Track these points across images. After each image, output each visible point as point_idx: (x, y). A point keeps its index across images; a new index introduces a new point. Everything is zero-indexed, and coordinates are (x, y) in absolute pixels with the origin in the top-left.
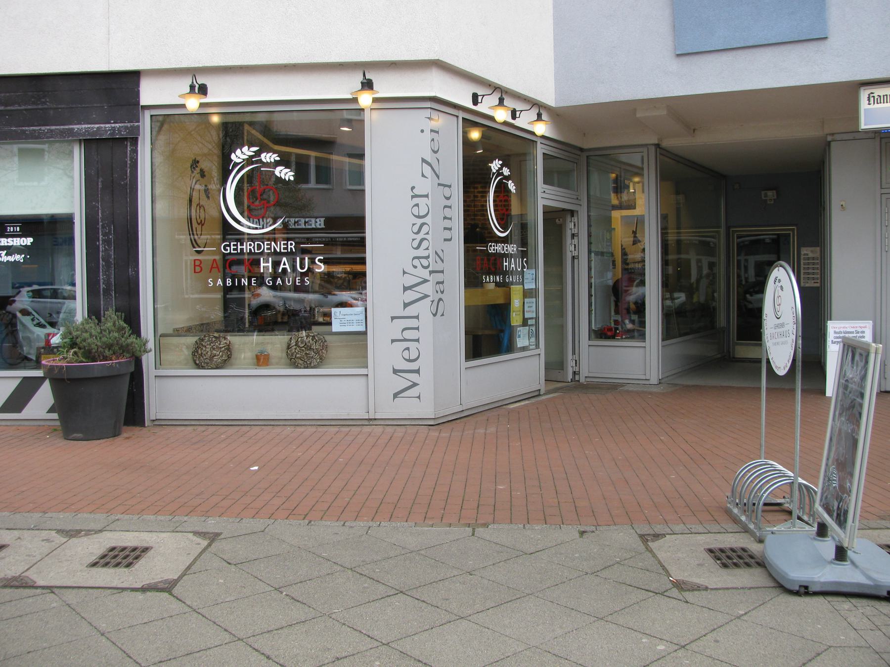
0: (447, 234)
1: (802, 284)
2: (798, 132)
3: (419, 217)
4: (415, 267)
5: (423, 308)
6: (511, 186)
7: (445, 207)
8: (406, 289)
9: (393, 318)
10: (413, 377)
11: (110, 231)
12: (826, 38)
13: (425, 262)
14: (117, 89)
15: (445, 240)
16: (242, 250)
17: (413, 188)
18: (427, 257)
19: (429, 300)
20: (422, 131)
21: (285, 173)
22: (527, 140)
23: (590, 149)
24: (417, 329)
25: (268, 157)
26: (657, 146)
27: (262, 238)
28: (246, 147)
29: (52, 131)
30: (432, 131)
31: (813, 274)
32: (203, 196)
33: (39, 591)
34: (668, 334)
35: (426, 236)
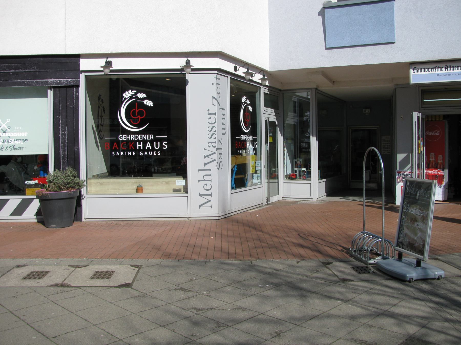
0: (223, 132)
1: (382, 153)
2: (381, 86)
3: (211, 124)
4: (210, 147)
5: (214, 166)
6: (250, 108)
7: (223, 119)
8: (205, 157)
9: (199, 170)
10: (209, 198)
11: (65, 129)
12: (393, 43)
13: (214, 145)
14: (69, 62)
15: (223, 134)
16: (128, 139)
17: (208, 110)
18: (215, 142)
19: (216, 162)
20: (213, 84)
21: (148, 103)
22: (256, 87)
23: (283, 91)
24: (211, 175)
25: (141, 95)
26: (316, 89)
27: (138, 133)
28: (130, 91)
29: (37, 82)
30: (217, 84)
31: (387, 148)
32: (103, 112)
33: (74, 288)
34: (322, 176)
35: (214, 133)
